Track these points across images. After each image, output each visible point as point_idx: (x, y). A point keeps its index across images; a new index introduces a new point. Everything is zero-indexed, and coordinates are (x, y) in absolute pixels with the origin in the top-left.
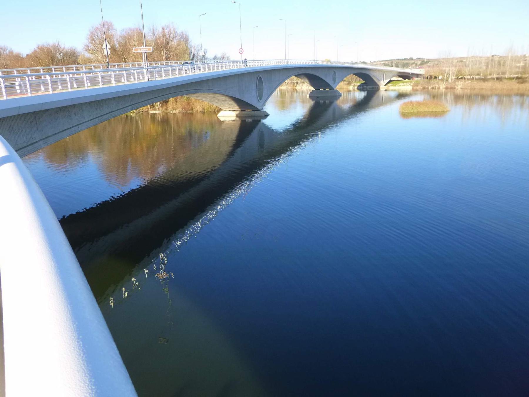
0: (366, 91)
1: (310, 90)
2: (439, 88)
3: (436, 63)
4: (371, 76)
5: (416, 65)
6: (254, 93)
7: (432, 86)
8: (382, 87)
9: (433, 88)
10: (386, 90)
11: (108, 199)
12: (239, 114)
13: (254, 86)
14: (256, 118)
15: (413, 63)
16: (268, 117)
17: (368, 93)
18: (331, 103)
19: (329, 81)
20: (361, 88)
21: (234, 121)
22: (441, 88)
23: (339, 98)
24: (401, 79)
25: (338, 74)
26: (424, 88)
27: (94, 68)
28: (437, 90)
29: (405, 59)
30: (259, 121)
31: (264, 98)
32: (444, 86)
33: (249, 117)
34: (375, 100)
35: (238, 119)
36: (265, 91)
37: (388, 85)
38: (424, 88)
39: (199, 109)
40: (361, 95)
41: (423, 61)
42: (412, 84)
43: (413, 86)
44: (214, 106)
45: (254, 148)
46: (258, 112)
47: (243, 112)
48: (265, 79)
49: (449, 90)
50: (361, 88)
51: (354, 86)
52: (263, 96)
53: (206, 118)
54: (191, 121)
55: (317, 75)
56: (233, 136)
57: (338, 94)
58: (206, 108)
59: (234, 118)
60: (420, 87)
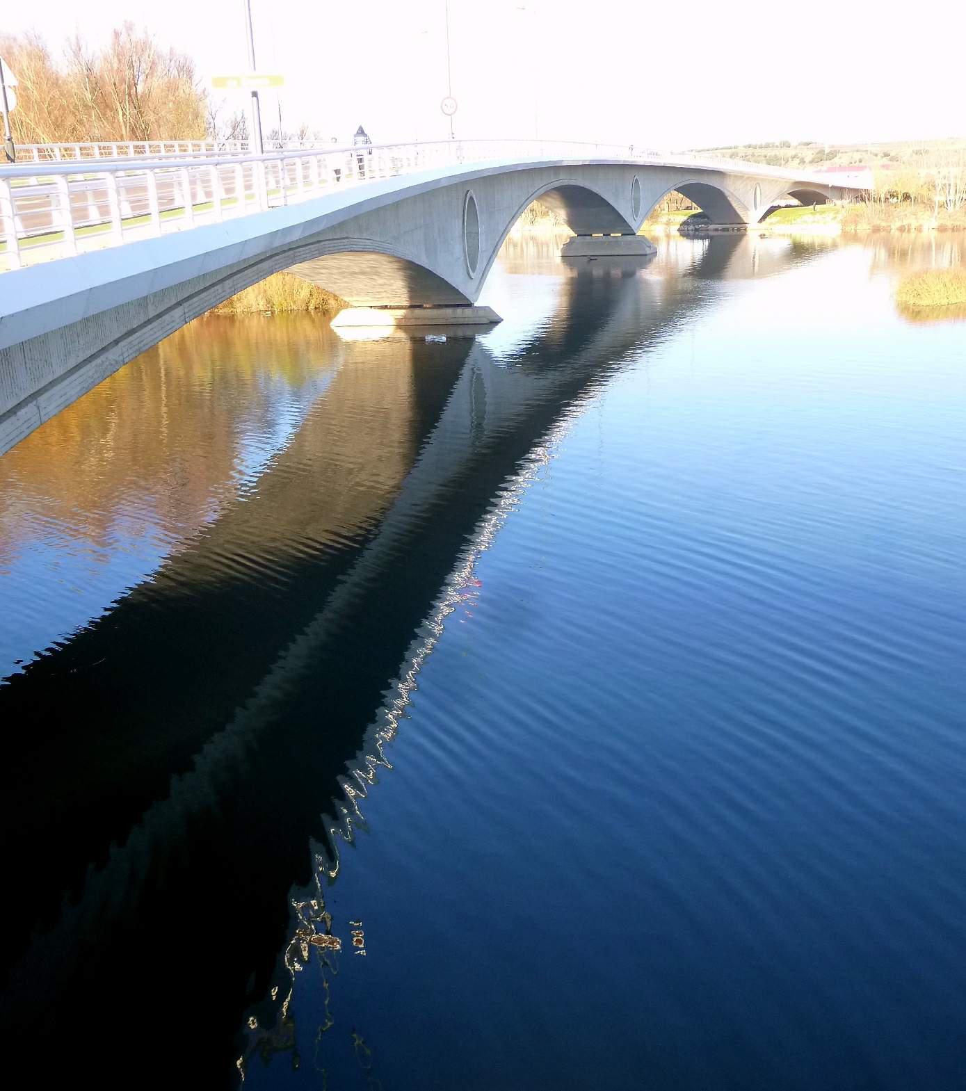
0: (703, 238)
1: (560, 236)
2: (919, 229)
3: (857, 156)
4: (727, 194)
5: (802, 161)
6: (458, 250)
7: (898, 224)
8: (753, 228)
9: (902, 229)
10: (762, 236)
11: (86, 625)
12: (405, 318)
13: (456, 227)
14: (460, 333)
15: (793, 157)
16: (497, 330)
17: (710, 245)
18: (629, 275)
19: (624, 210)
20: (690, 230)
21: (386, 340)
22: (925, 228)
23: (650, 261)
24: (795, 202)
25: (646, 184)
26: (876, 229)
27: (41, 157)
28: (913, 234)
29: (767, 146)
30: (470, 341)
31: (480, 265)
32: (935, 224)
33: (436, 327)
34: (737, 261)
35: (402, 335)
36: (483, 245)
37: (767, 220)
38: (876, 229)
39: (253, 302)
40: (698, 249)
41: (822, 152)
42: (840, 217)
43: (844, 223)
44: (304, 293)
45: (471, 426)
46: (468, 311)
47: (418, 312)
48: (477, 202)
49: (949, 233)
50: (690, 230)
51: (668, 224)
52: (477, 262)
53: (279, 333)
54: (226, 344)
55: (595, 189)
56: (397, 391)
57: (648, 251)
58: (276, 300)
59: (389, 332)
60: (864, 228)
